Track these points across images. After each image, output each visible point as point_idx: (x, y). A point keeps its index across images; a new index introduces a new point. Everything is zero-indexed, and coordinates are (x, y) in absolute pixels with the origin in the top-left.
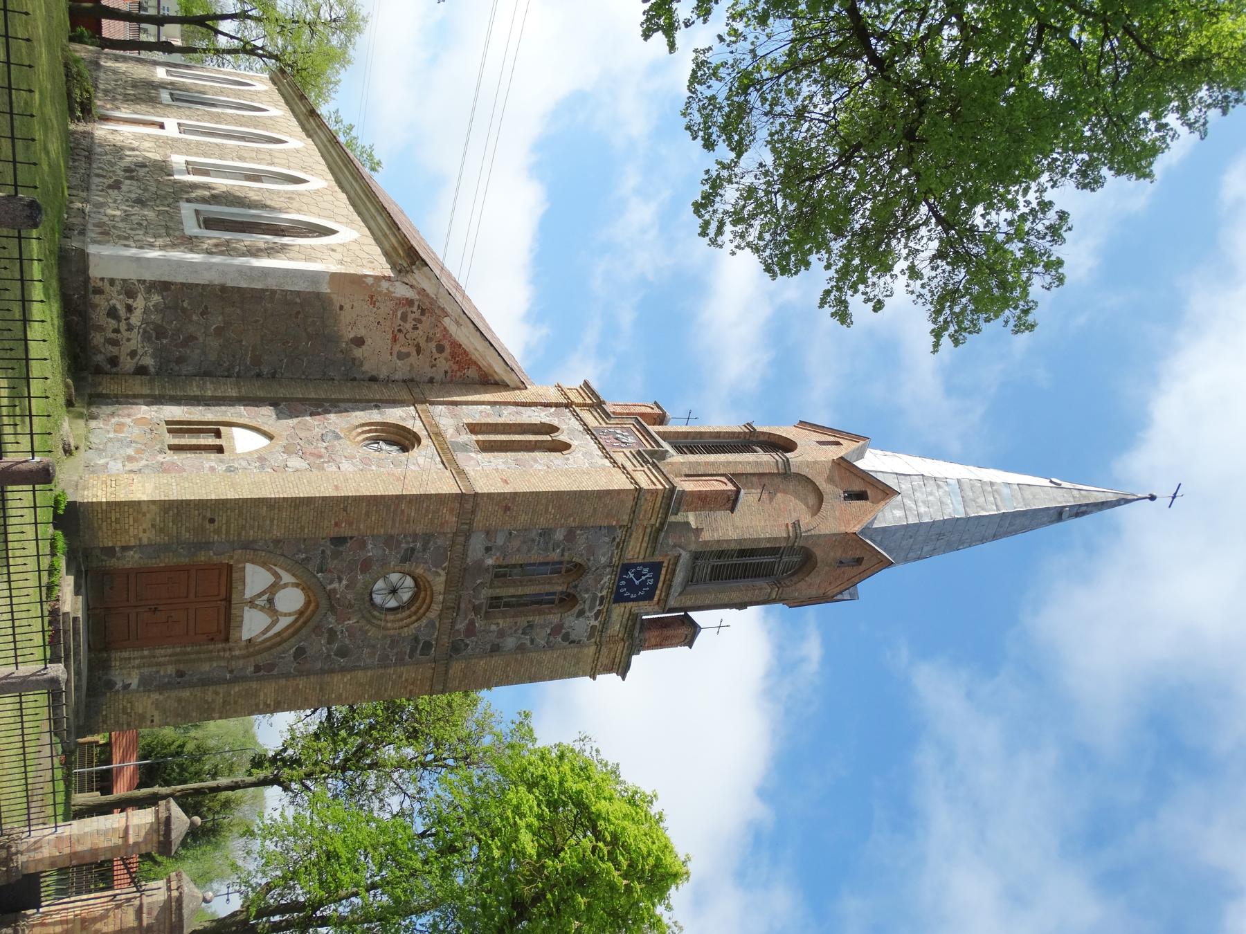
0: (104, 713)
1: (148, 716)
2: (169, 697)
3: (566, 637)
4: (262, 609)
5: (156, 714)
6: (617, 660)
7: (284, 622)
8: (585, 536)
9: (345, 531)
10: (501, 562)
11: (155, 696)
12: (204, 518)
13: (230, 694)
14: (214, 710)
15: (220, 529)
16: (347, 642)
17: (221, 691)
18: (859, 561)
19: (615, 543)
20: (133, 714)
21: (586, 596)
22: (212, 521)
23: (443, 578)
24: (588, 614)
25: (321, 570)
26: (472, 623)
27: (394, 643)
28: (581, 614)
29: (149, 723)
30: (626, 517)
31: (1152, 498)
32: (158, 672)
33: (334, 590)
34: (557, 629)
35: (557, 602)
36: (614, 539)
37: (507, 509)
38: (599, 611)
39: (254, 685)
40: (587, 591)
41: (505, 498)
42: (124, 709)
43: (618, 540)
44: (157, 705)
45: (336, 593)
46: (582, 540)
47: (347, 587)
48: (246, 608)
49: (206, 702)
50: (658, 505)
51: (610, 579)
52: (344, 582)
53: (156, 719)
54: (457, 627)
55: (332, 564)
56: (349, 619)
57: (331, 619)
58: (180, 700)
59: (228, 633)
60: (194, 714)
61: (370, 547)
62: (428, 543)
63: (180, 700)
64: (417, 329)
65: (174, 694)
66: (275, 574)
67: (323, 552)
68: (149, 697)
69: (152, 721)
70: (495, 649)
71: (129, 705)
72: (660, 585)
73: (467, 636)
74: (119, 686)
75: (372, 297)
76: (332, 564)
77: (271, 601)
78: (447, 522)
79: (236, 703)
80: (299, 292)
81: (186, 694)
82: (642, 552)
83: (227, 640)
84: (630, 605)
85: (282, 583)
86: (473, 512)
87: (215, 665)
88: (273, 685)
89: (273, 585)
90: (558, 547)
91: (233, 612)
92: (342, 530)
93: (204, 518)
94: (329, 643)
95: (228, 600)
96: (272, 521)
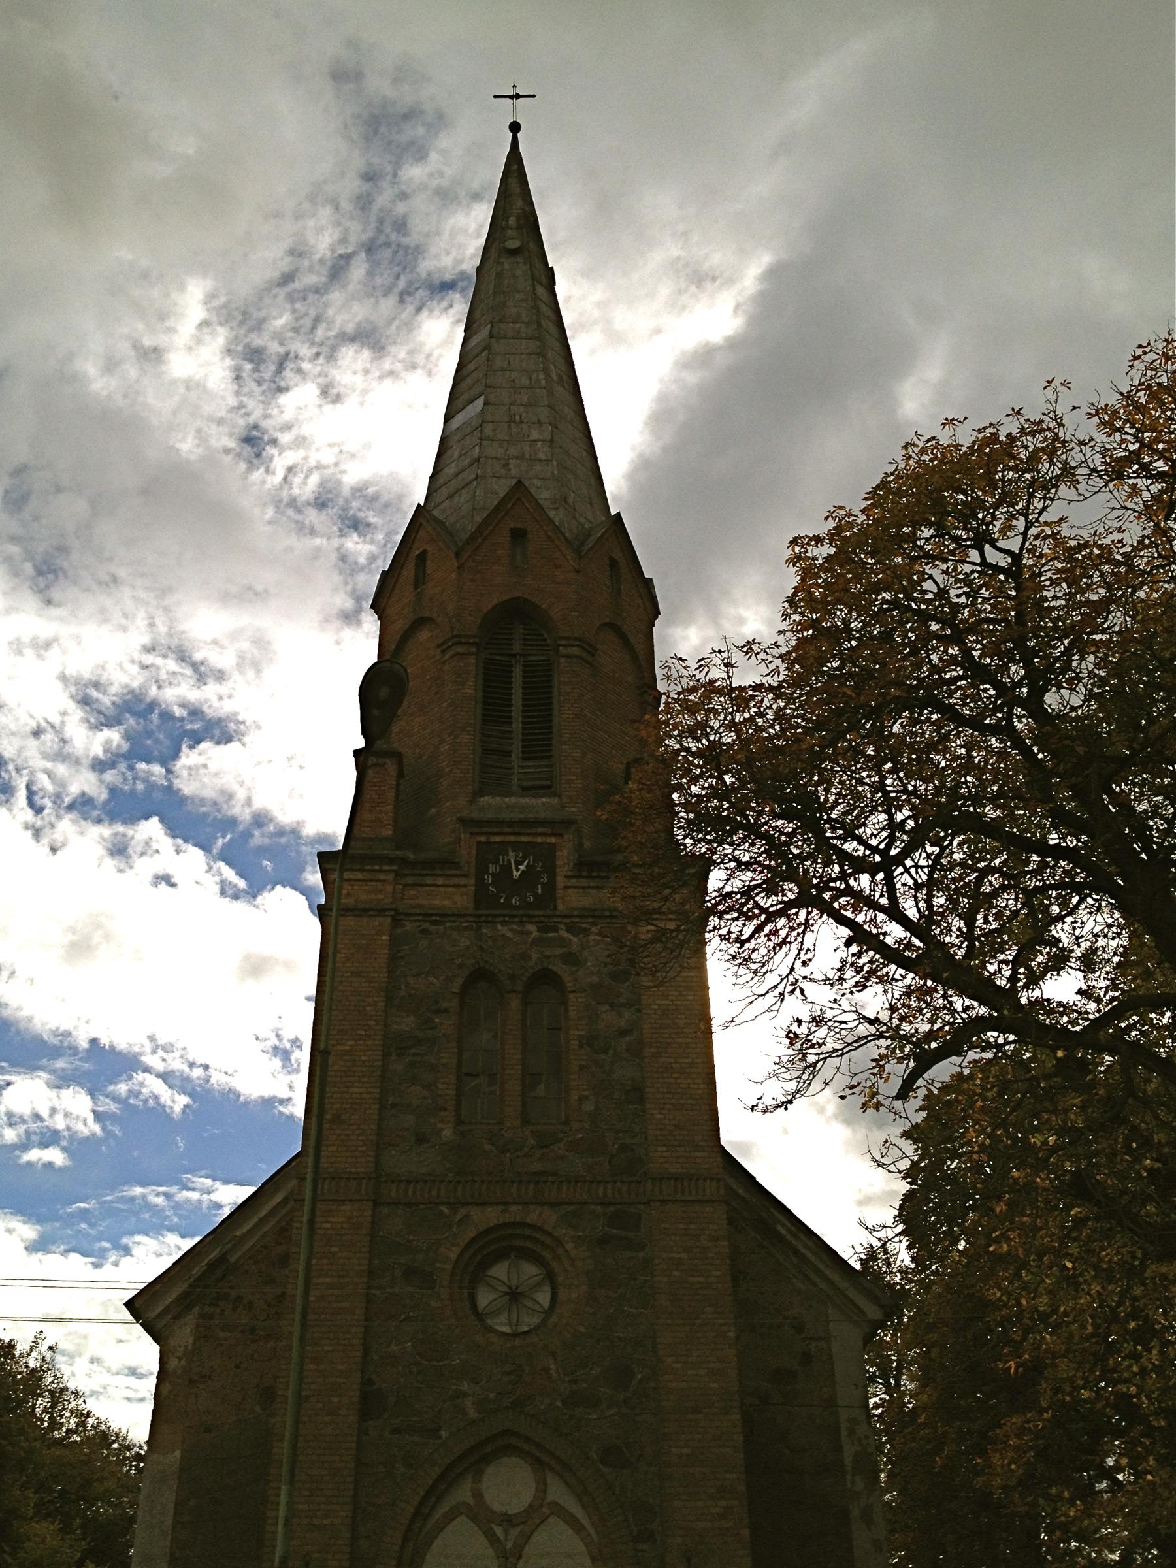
4: (527, 1537)
7: (557, 1492)
18: (518, 535)
21: (535, 956)
23: (476, 1214)
30: (377, 922)
36: (424, 931)
50: (359, 876)
51: (503, 923)
52: (465, 1386)
64: (250, 1303)
66: (450, 1517)
67: (396, 1431)
70: (637, 1094)
75: (191, 1381)
77: (508, 1520)
80: (176, 1504)
82: (456, 881)
84: (560, 881)
89: (474, 1518)
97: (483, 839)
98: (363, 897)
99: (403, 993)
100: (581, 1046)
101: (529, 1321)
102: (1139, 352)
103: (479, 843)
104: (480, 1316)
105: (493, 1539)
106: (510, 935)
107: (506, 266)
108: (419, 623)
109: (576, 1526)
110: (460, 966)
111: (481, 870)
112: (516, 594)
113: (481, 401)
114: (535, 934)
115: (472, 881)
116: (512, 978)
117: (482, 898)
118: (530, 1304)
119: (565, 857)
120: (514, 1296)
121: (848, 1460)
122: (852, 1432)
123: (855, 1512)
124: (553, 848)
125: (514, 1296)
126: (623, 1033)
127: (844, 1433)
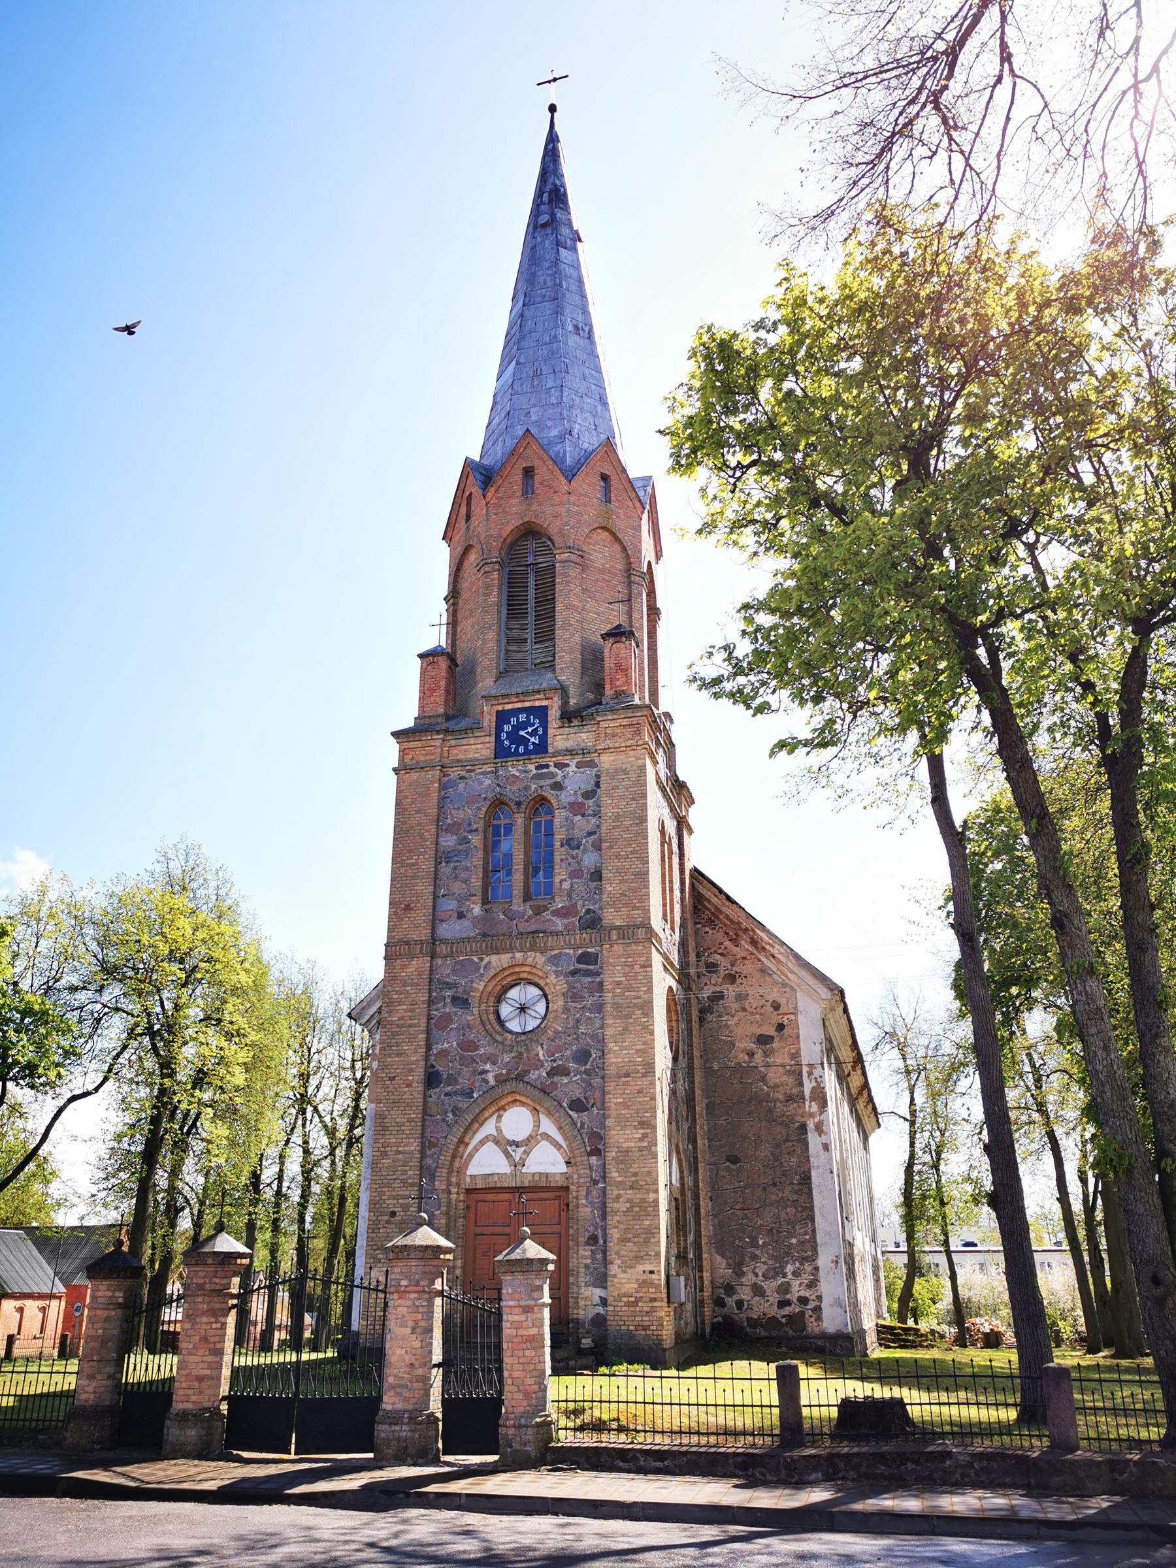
0: (632, 1328)
1: (645, 1277)
2: (617, 1253)
3: (589, 795)
4: (527, 1153)
5: (640, 1268)
6: (625, 722)
7: (548, 1126)
8: (454, 812)
9: (418, 1076)
10: (478, 899)
11: (614, 1269)
12: (388, 1222)
13: (622, 1183)
14: (643, 1200)
15: (402, 1206)
16: (568, 1053)
17: (615, 1193)
19: (467, 775)
20: (638, 1295)
21: (533, 787)
22: (393, 1214)
23: (494, 958)
24: (559, 779)
25: (470, 1095)
26: (557, 913)
27: (575, 997)
28: (557, 786)
29: (653, 1276)
31: (552, 109)
32: (587, 1266)
33: (496, 1077)
34: (576, 808)
35: (549, 818)
37: (408, 908)
38: (556, 765)
39: (611, 1154)
40: (527, 788)
41: (396, 913)
42: (628, 1304)
43: (463, 773)
44: (626, 1267)
45: (501, 1074)
46: (457, 814)
47: (494, 1063)
48: (524, 1170)
49: (630, 1210)
50: (418, 744)
52: (488, 1067)
53: (649, 1268)
54: (560, 928)
55: (464, 1083)
56: (537, 1055)
57: (533, 1076)
58: (623, 1240)
59: (561, 1187)
60: (647, 1223)
61: (446, 1045)
62: (448, 983)
63: (623, 1240)
65: (612, 1245)
66: (482, 1143)
67: (447, 1094)
68: (615, 1276)
69: (652, 1272)
70: (597, 875)
71: (625, 1299)
72: (527, 704)
73: (576, 913)
74: (600, 1310)
76: (464, 1083)
77: (516, 1144)
78: (416, 970)
79: (635, 1175)
81: (614, 1234)
82: (482, 740)
83: (567, 1189)
85: (495, 1134)
86: (408, 943)
87: (584, 1201)
88: (613, 1132)
89: (497, 1142)
90: (465, 837)
91: (526, 1184)
92: (416, 1078)
93: (388, 1222)
94: (568, 1074)
95: (520, 1190)
96: (399, 1152)
97: (500, 708)
98: (422, 758)
99: (449, 821)
100: (562, 846)
101: (532, 1024)
102: (670, 403)
103: (497, 712)
104: (501, 1022)
105: (507, 1155)
106: (517, 774)
107: (539, 239)
108: (467, 549)
109: (558, 1146)
110: (485, 799)
111: (499, 729)
112: (526, 519)
113: (514, 363)
114: (534, 772)
115: (493, 739)
116: (519, 804)
117: (501, 752)
118: (533, 1014)
119: (554, 713)
120: (523, 1009)
121: (807, 1093)
122: (810, 1074)
123: (811, 1125)
124: (545, 709)
125: (523, 1009)
126: (590, 834)
127: (805, 1074)
